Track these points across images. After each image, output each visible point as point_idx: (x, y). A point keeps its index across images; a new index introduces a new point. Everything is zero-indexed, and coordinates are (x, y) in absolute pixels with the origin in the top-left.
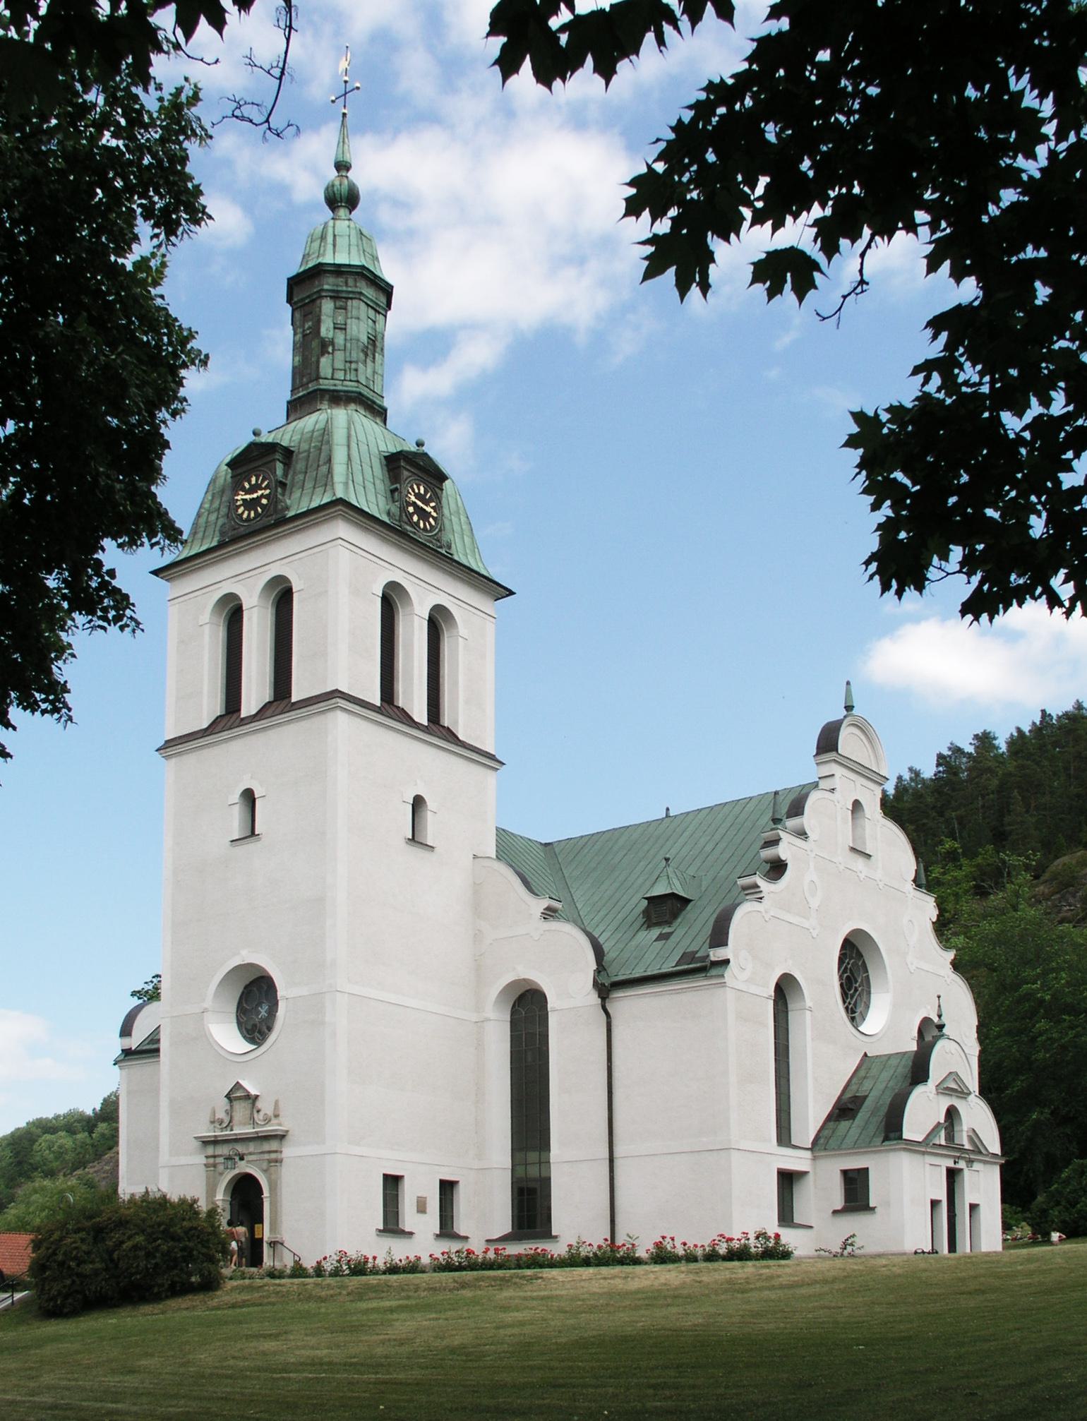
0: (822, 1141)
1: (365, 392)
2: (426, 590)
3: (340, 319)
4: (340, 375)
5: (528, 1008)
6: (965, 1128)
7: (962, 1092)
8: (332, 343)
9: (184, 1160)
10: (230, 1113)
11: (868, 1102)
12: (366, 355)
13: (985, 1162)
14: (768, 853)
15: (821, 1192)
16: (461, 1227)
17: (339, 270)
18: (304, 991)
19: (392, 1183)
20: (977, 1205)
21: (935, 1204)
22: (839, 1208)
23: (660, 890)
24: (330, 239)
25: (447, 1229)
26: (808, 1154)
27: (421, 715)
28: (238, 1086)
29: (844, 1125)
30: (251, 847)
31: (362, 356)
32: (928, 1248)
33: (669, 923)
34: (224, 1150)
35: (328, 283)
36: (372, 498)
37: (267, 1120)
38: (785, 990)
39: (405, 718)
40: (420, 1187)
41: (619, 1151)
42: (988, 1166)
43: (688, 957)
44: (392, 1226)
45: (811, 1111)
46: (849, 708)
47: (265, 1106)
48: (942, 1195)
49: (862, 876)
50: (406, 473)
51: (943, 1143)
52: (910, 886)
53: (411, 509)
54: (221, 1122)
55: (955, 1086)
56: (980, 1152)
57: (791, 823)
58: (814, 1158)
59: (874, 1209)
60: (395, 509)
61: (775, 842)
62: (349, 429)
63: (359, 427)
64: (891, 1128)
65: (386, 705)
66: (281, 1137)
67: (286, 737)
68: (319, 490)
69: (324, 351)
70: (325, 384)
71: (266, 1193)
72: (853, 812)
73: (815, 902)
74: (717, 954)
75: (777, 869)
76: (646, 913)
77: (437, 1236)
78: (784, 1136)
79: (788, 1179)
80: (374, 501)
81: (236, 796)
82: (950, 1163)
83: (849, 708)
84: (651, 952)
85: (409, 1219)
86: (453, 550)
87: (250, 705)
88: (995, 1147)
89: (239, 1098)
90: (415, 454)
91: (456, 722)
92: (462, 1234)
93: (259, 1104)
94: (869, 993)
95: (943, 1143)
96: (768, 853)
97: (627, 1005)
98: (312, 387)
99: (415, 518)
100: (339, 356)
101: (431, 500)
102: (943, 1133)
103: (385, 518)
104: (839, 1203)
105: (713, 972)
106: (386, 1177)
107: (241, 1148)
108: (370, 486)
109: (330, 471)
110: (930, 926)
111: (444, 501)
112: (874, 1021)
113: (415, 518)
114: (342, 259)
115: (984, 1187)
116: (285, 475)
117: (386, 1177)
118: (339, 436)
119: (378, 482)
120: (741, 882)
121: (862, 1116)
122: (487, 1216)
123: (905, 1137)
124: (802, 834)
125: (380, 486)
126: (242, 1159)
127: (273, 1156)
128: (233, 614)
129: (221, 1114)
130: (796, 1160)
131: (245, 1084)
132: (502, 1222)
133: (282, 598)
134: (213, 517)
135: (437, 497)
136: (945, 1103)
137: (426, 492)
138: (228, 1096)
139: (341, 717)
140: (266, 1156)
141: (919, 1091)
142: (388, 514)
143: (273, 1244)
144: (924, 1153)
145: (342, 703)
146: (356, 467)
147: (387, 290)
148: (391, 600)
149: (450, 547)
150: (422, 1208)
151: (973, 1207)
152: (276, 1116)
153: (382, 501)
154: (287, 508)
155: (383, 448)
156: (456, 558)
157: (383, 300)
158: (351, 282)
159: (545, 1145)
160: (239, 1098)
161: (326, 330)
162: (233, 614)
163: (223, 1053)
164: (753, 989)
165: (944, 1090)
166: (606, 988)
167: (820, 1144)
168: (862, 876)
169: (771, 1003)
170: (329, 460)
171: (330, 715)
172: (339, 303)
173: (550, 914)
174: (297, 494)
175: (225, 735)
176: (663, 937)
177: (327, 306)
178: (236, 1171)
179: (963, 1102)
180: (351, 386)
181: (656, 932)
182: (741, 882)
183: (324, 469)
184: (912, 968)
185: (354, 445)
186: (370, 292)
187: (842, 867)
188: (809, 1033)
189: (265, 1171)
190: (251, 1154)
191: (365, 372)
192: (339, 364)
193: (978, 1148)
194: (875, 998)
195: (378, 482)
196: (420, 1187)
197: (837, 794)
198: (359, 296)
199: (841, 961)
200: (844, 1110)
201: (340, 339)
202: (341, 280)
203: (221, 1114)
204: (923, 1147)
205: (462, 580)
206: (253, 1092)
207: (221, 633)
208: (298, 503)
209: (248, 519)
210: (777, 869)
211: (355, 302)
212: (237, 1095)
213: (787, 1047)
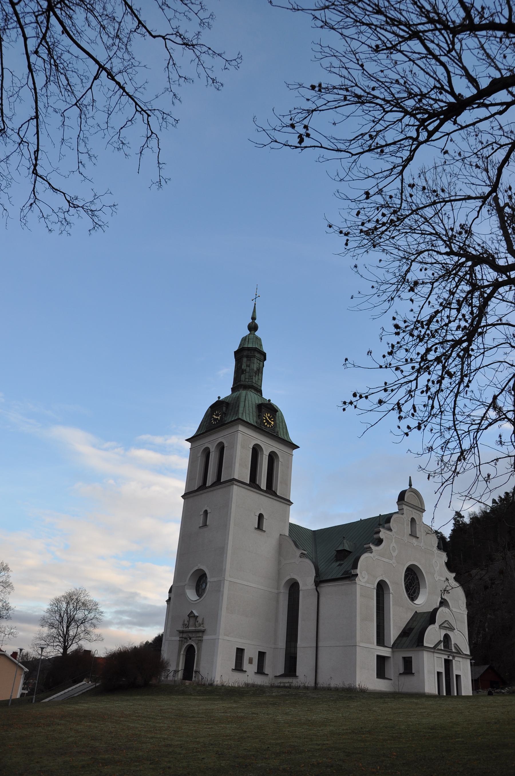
0: (396, 645)
1: (255, 385)
2: (268, 446)
3: (248, 363)
4: (247, 380)
5: (294, 588)
6: (453, 643)
7: (451, 629)
8: (245, 370)
9: (174, 638)
10: (188, 622)
11: (414, 631)
12: (256, 374)
13: (463, 658)
14: (376, 536)
15: (395, 667)
16: (267, 670)
17: (249, 349)
18: (215, 579)
19: (240, 652)
20: (460, 676)
21: (439, 674)
22: (402, 672)
23: (340, 548)
24: (247, 340)
25: (260, 671)
26: (390, 650)
27: (264, 486)
28: (192, 612)
29: (405, 639)
30: (205, 529)
31: (254, 374)
32: (312, 684)
33: (343, 560)
34: (185, 635)
35: (245, 353)
36: (251, 418)
37: (200, 625)
38: (382, 588)
39: (258, 488)
40: (251, 653)
41: (320, 644)
42: (465, 660)
43: (346, 572)
44: (239, 667)
45: (393, 633)
46: (410, 485)
47: (200, 620)
48: (442, 670)
49: (415, 545)
50: (263, 410)
51: (442, 648)
52: (435, 549)
53: (265, 421)
54: (186, 625)
55: (448, 626)
56: (460, 654)
57: (386, 525)
58: (393, 652)
59: (414, 674)
60: (259, 421)
61: (379, 532)
62: (246, 396)
63: (249, 396)
64: (419, 642)
65: (252, 483)
66: (203, 632)
67: (217, 494)
68: (235, 416)
69: (242, 373)
70: (242, 383)
71: (196, 653)
72: (411, 522)
73: (394, 554)
74: (353, 572)
75: (380, 542)
76: (336, 556)
77: (255, 673)
78: (381, 641)
79: (381, 660)
80: (251, 419)
81: (202, 513)
82: (446, 657)
83: (410, 485)
84: (336, 570)
85: (246, 666)
86: (279, 434)
87: (209, 483)
88: (468, 653)
89: (192, 617)
90: (267, 404)
91: (277, 489)
92: (266, 673)
93: (198, 619)
94: (419, 588)
95: (442, 648)
96: (376, 536)
97: (327, 589)
98: (238, 384)
99: (266, 424)
100: (247, 374)
101: (272, 418)
102: (442, 644)
103: (255, 424)
104: (402, 671)
105: (353, 578)
106: (238, 649)
107: (190, 635)
108: (251, 414)
109: (238, 410)
110: (444, 564)
111: (277, 418)
112: (420, 600)
113: (266, 424)
114: (250, 346)
115: (463, 669)
116: (226, 411)
117: (238, 649)
118: (242, 399)
119: (254, 413)
120: (365, 546)
121: (412, 635)
122: (276, 665)
123: (424, 645)
124: (390, 530)
125: (255, 414)
126: (190, 639)
127: (200, 638)
128: (207, 453)
129: (186, 622)
130: (385, 652)
131: (194, 612)
132: (281, 670)
133: (221, 448)
134: (205, 424)
135: (274, 417)
136: (443, 632)
137: (270, 416)
138: (188, 616)
139: (235, 487)
140: (198, 638)
141: (431, 627)
142: (257, 422)
143: (196, 672)
144: (434, 652)
145: (235, 483)
146: (247, 408)
147: (264, 355)
148: (256, 451)
149: (278, 433)
150: (251, 661)
151: (458, 677)
152: (203, 624)
153: (255, 419)
154: (225, 421)
155: (257, 402)
156: (280, 436)
157: (263, 357)
158: (252, 353)
159: (296, 641)
160: (192, 617)
161: (244, 367)
162: (207, 453)
163: (189, 600)
164: (368, 585)
165: (441, 627)
166: (318, 582)
167: (395, 646)
168: (415, 545)
169: (375, 591)
170: (238, 406)
171: (231, 486)
172: (249, 359)
173: (302, 555)
174: (228, 417)
175: (201, 492)
176: (340, 565)
177: (245, 360)
178: (188, 644)
179: (452, 632)
180: (250, 383)
181: (338, 563)
182: (365, 546)
183: (237, 409)
184: (437, 579)
185: (247, 402)
186: (258, 355)
187: (406, 542)
188: (391, 603)
189: (197, 644)
190: (193, 637)
191: (255, 379)
192: (247, 377)
193: (459, 652)
194: (421, 590)
195: (254, 413)
196: (251, 653)
197: (404, 516)
198: (254, 357)
199: (406, 576)
200: (405, 633)
201: (248, 369)
202: (249, 352)
203: (186, 622)
204: (434, 649)
205: (281, 443)
206: (196, 614)
207: (204, 460)
208: (229, 419)
209: (214, 424)
210: (380, 542)
211: (253, 358)
212: (191, 615)
213: (384, 607)
